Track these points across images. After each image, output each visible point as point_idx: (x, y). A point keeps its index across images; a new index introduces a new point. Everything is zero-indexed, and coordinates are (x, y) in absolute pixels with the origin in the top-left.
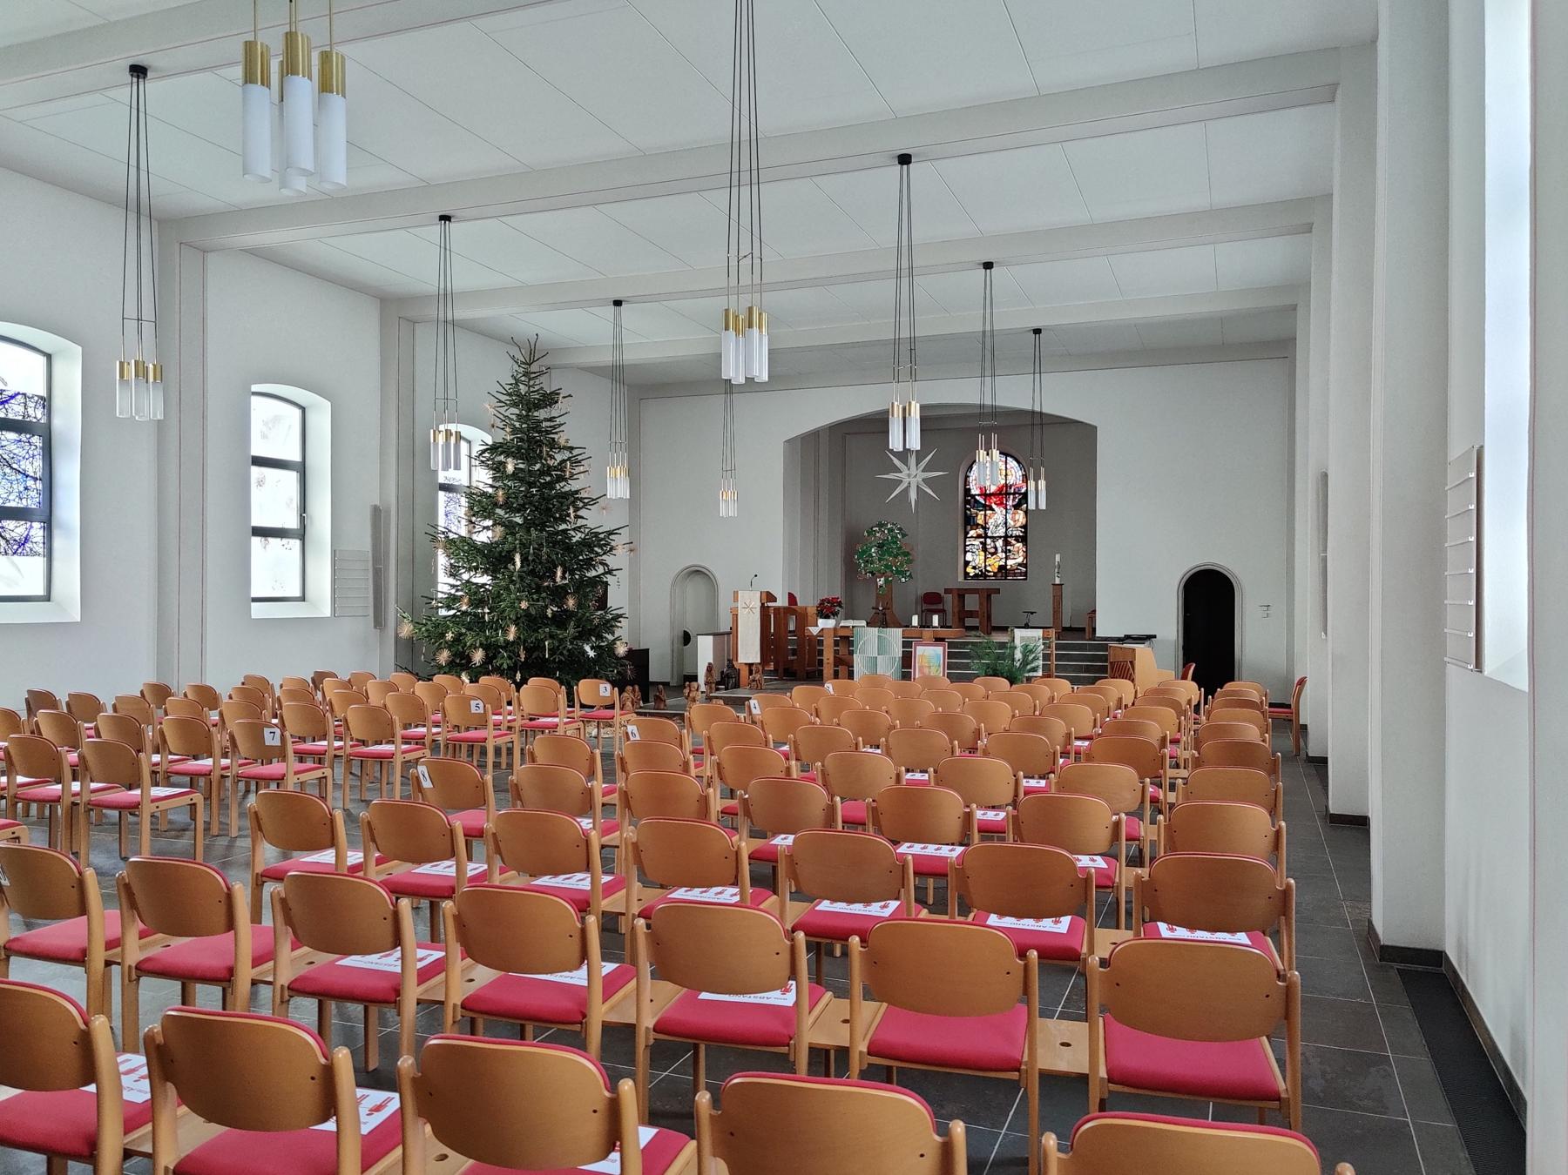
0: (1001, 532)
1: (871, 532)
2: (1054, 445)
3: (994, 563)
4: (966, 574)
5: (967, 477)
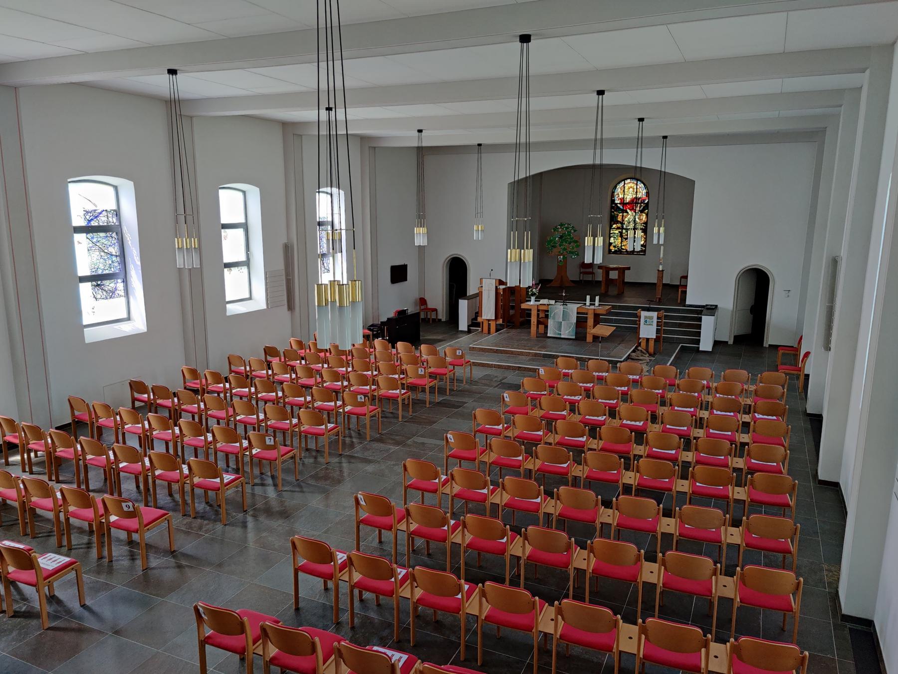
1: (556, 229)
2: (670, 196)
4: (610, 251)
5: (613, 192)
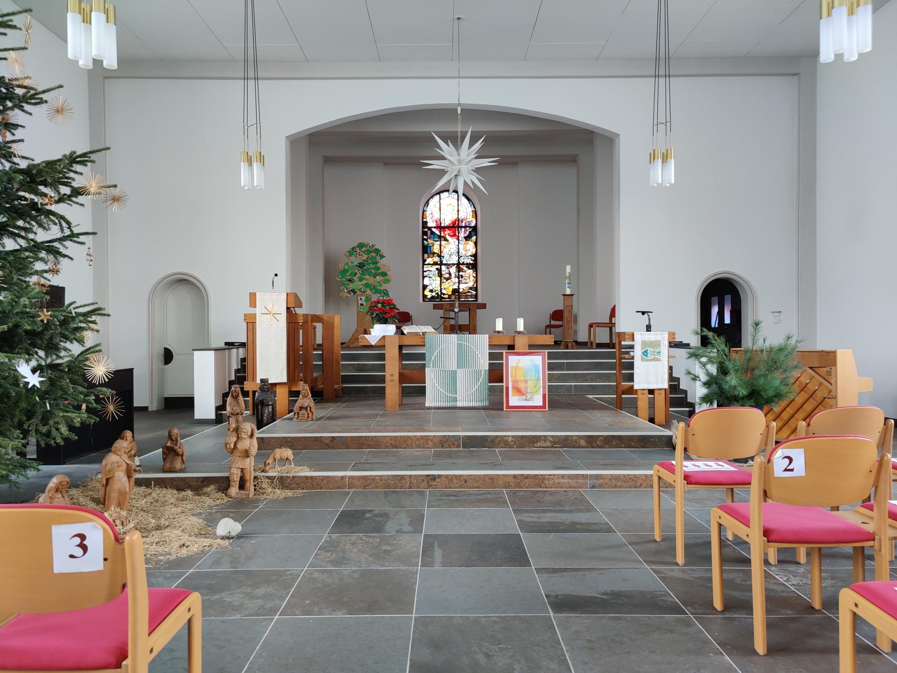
0: (454, 260)
3: (448, 287)
4: (424, 296)
5: (424, 211)
